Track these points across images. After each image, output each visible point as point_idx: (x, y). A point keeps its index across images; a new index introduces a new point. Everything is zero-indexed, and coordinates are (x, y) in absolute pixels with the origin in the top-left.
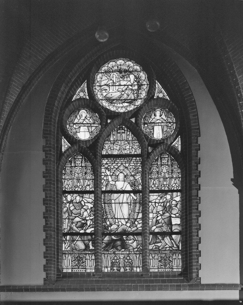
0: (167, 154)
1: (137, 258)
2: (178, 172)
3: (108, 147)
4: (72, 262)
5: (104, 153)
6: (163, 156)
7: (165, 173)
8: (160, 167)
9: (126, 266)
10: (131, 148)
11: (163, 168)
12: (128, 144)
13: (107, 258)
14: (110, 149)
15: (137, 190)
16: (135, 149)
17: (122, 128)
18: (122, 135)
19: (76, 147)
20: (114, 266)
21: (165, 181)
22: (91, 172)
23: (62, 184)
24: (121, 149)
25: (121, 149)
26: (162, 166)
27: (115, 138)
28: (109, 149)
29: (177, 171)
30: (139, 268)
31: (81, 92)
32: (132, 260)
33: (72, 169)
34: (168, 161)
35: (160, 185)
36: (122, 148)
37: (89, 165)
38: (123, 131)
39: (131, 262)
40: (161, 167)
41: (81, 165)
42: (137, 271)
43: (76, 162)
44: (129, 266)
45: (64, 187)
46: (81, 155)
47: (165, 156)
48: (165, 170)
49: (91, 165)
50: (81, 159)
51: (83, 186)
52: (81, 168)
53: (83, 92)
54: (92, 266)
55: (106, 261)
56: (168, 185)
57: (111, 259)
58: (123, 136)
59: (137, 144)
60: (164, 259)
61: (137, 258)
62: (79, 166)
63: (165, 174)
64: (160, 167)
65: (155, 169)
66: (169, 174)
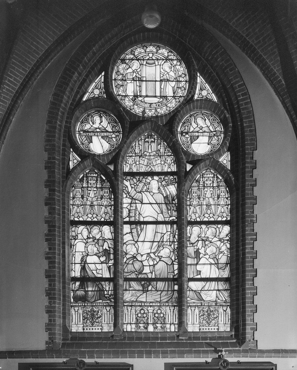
0: (211, 172)
1: (128, 311)
2: (227, 197)
3: (171, 160)
4: (218, 316)
5: (126, 169)
6: (91, 174)
7: (209, 198)
8: (202, 189)
9: (156, 322)
10: (163, 163)
11: (207, 191)
12: (159, 158)
13: (131, 311)
14: (135, 164)
15: (137, 220)
16: (130, 165)
17: (151, 135)
18: (150, 145)
19: (88, 162)
20: (140, 322)
21: (92, 209)
22: (109, 196)
23: (69, 211)
24: (149, 163)
25: (149, 163)
26: (205, 188)
27: (142, 150)
28: (172, 163)
29: (225, 195)
30: (174, 325)
31: (96, 89)
32: (164, 315)
33: (200, 191)
34: (213, 182)
35: (85, 214)
36: (151, 163)
37: (107, 186)
38: (153, 140)
39: (146, 317)
40: (203, 190)
41: (96, 186)
42: (171, 331)
43: (89, 182)
44: (143, 323)
45: (73, 215)
46: (95, 172)
47: (92, 175)
48: (208, 195)
49: (109, 187)
50: (212, 177)
51: (98, 215)
52: (95, 189)
53: (99, 89)
54: (110, 323)
55: (172, 316)
56: (96, 215)
57: (136, 313)
58: (153, 146)
59: (171, 157)
60: (208, 314)
61: (171, 312)
62: (93, 187)
63: (209, 199)
64: (202, 190)
65: (196, 193)
66: (98, 200)
